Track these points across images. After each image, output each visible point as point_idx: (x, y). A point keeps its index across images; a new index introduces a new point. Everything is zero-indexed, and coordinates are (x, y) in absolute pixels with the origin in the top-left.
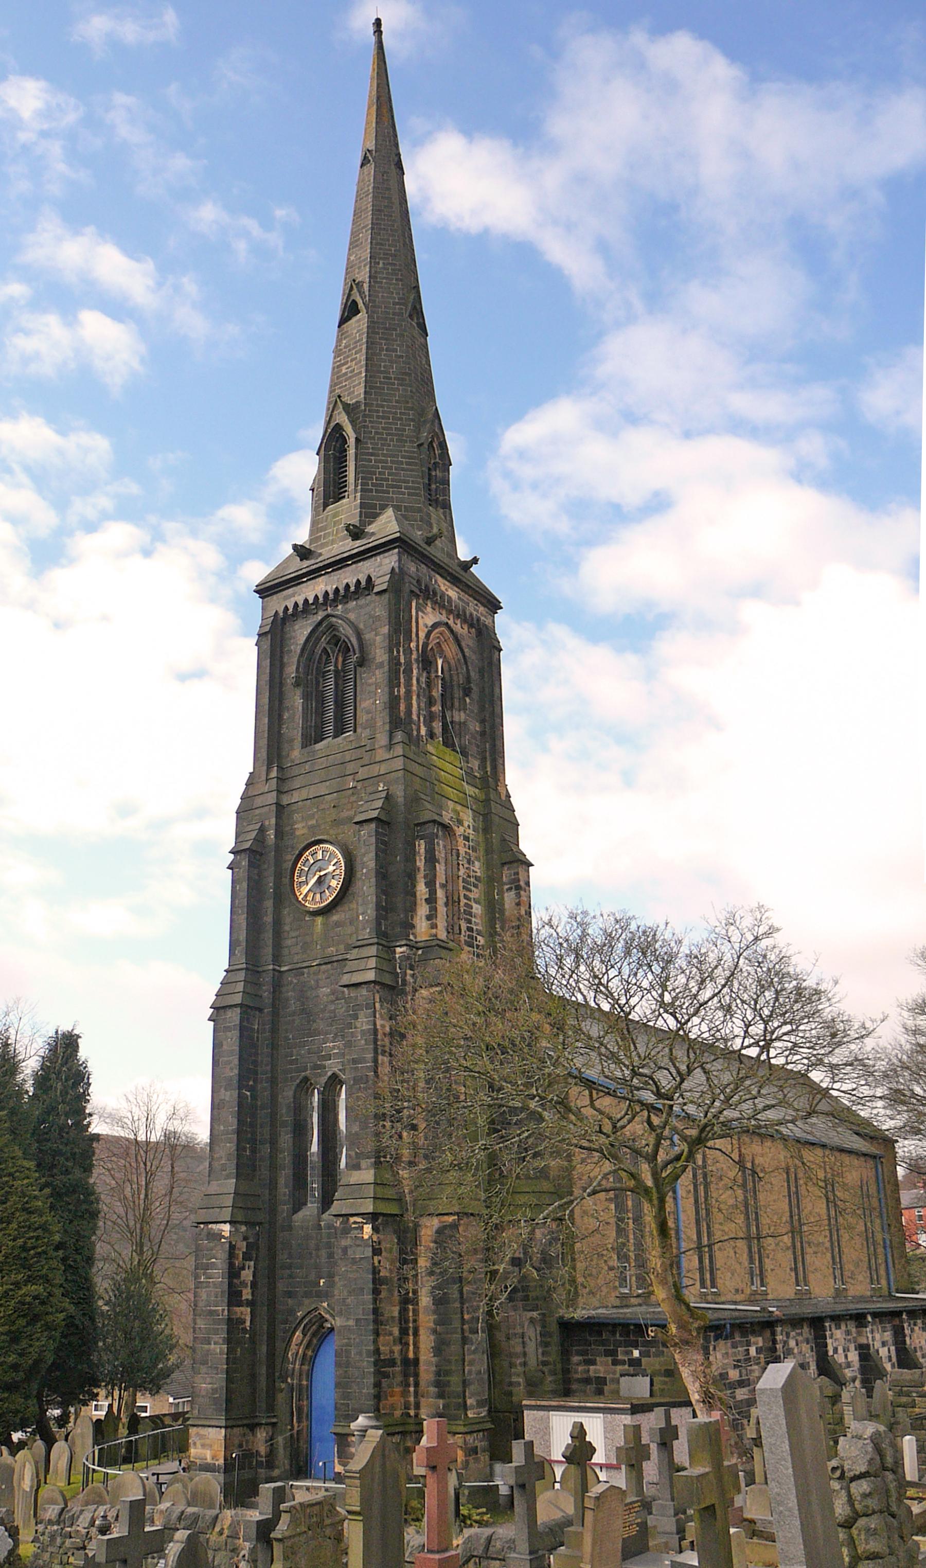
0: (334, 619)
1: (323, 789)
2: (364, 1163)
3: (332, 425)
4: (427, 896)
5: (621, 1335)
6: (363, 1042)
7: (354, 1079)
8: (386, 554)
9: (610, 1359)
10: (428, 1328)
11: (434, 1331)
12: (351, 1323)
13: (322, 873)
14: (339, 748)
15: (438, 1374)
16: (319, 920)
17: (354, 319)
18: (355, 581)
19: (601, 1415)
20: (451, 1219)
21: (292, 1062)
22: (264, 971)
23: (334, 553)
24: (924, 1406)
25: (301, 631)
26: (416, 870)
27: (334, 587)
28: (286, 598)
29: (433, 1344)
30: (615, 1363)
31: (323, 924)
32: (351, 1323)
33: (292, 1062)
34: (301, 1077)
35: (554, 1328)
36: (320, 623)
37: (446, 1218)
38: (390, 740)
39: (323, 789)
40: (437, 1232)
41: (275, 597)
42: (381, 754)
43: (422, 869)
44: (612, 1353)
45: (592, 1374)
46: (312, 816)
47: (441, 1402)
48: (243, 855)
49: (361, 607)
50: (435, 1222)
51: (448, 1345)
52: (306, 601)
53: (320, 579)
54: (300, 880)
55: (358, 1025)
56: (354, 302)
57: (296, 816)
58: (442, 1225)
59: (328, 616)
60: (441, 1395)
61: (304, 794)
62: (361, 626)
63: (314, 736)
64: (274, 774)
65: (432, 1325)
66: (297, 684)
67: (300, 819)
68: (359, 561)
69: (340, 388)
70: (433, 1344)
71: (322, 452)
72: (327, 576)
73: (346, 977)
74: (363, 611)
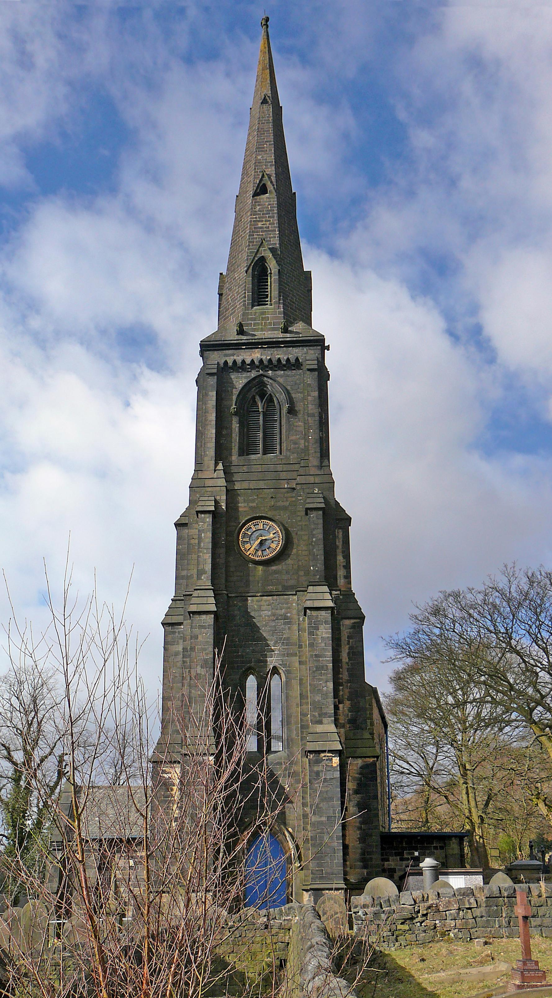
0: (265, 379)
1: (261, 484)
2: (325, 720)
3: (259, 255)
4: (345, 564)
5: (406, 844)
6: (323, 645)
7: (316, 667)
8: (311, 348)
9: (398, 857)
10: (355, 826)
11: (360, 828)
12: (324, 819)
13: (264, 538)
14: (271, 461)
15: (363, 853)
16: (260, 568)
17: (262, 196)
18: (285, 358)
19: (463, 876)
20: (371, 760)
21: (238, 656)
22: (220, 594)
23: (272, 336)
24: (21, 997)
25: (239, 381)
26: (336, 547)
27: (268, 358)
28: (226, 355)
29: (359, 836)
30: (402, 859)
31: (264, 571)
32: (324, 819)
33: (238, 656)
34: (246, 667)
35: (375, 840)
36: (254, 379)
37: (368, 759)
38: (321, 464)
39: (261, 484)
40: (361, 768)
41: (216, 352)
42: (313, 471)
43: (341, 547)
44: (401, 854)
45: (386, 866)
46: (253, 501)
47: (365, 871)
48: (207, 515)
49: (288, 376)
50: (360, 762)
51: (371, 836)
52: (243, 362)
53: (256, 350)
54: (244, 540)
55: (319, 633)
56: (264, 185)
57: (240, 499)
58: (364, 763)
59: (261, 375)
60: (365, 867)
61: (245, 485)
62: (289, 388)
63: (246, 449)
64: (220, 466)
65: (358, 824)
66: (236, 414)
67: (242, 501)
68: (273, 347)
69: (258, 235)
70: (359, 836)
71: (250, 270)
72: (262, 349)
73: (308, 602)
74: (290, 379)
